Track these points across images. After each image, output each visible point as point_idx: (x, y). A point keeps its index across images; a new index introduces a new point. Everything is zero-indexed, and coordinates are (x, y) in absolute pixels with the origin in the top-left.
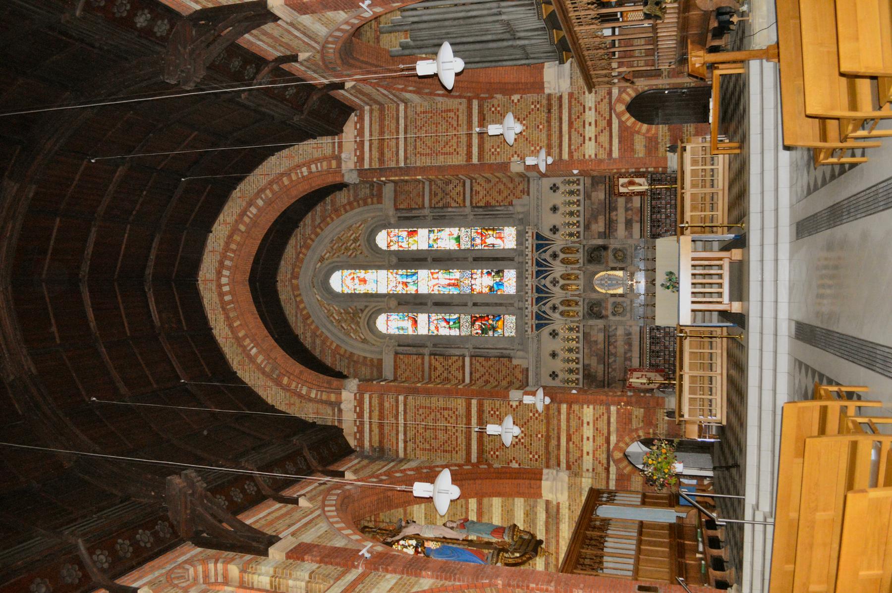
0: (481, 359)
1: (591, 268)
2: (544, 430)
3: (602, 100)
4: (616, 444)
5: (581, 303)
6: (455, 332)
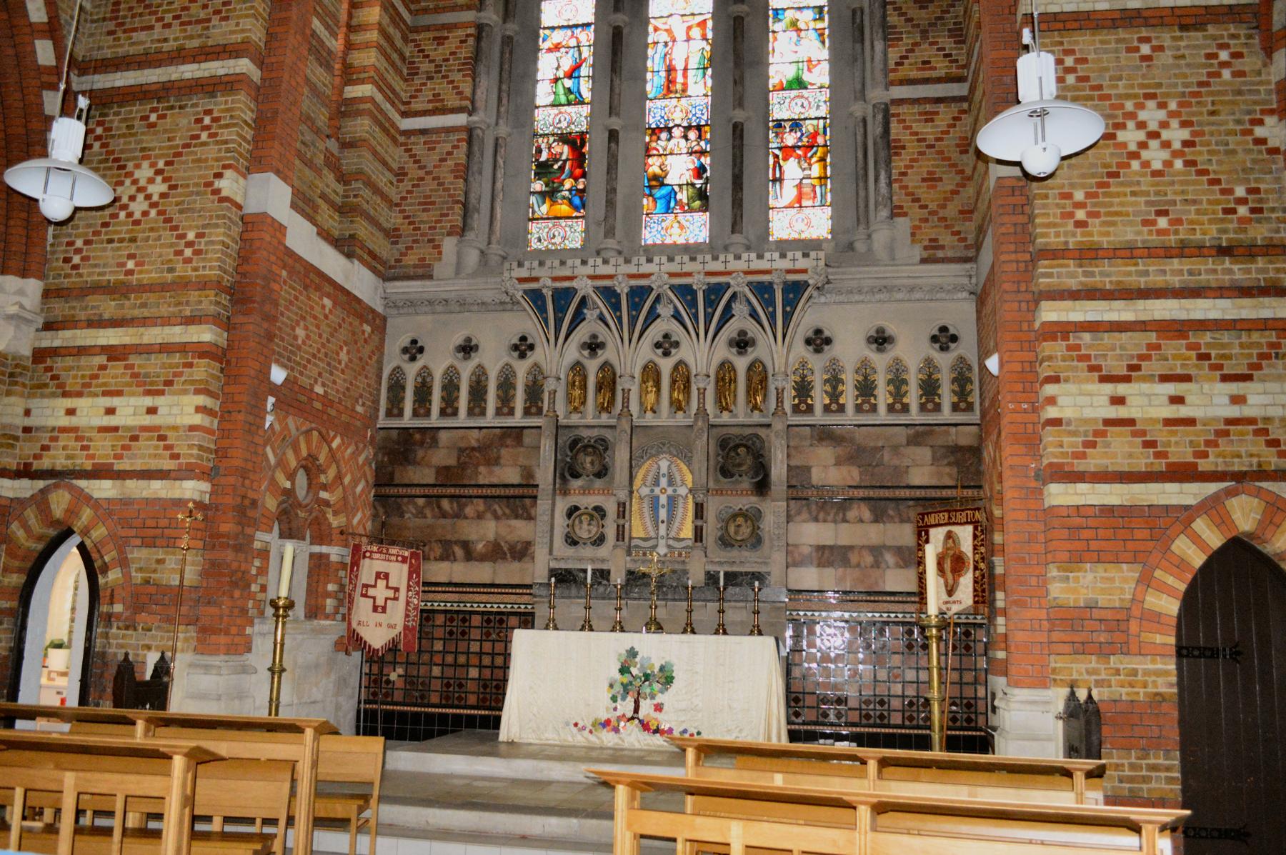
0: (460, 155)
1: (702, 445)
2: (145, 278)
4: (89, 498)
5: (605, 419)
6: (543, 93)
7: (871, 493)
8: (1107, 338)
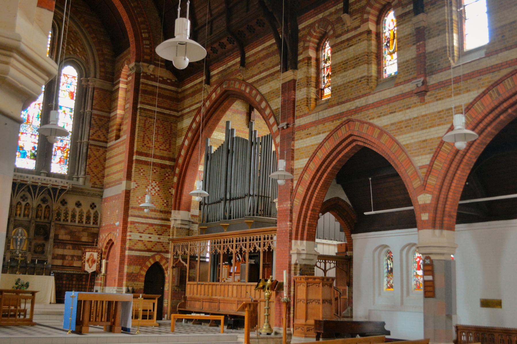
3: (164, 246)
7: (72, 242)
8: (140, 225)
